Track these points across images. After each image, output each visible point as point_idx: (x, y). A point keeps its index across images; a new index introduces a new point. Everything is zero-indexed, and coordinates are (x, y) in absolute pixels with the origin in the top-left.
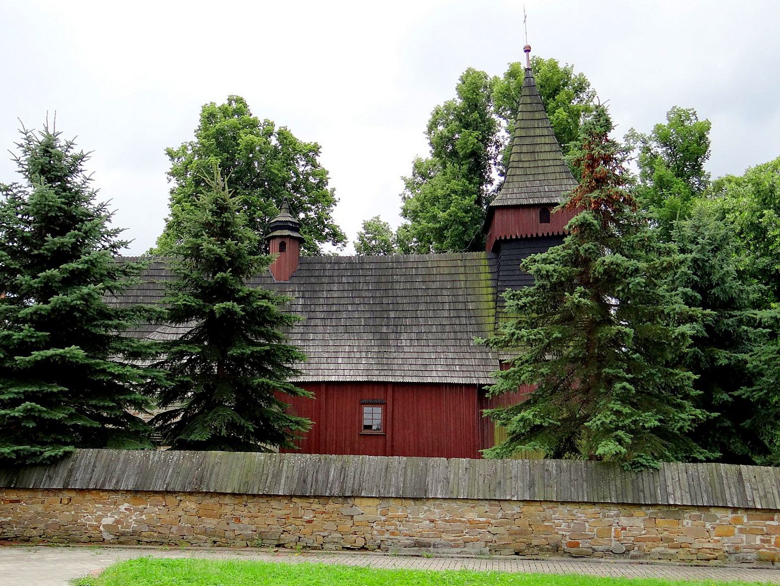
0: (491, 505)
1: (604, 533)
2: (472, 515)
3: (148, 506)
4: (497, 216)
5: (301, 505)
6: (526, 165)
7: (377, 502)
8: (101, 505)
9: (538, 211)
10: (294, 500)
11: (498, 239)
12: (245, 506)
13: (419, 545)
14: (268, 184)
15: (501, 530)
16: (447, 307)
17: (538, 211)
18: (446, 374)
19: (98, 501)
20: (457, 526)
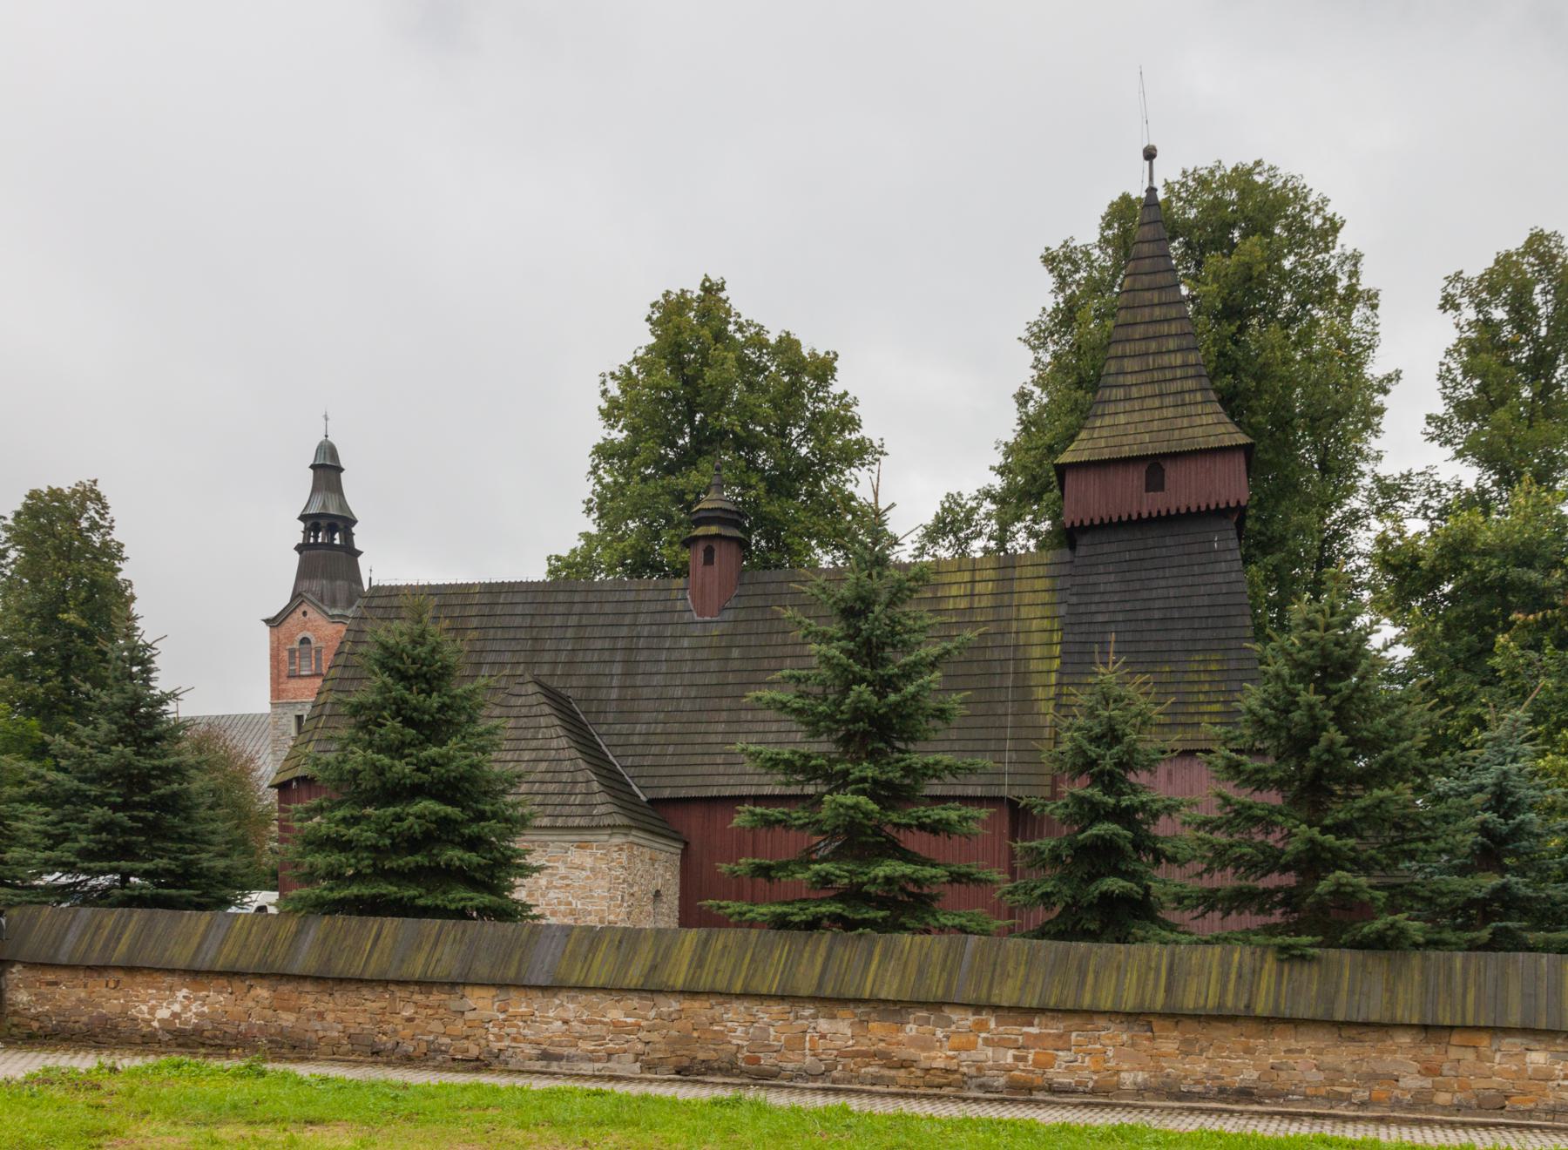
1: (795, 1043)
2: (616, 1014)
6: (1129, 379)
7: (493, 992)
9: (1143, 469)
13: (546, 1056)
15: (654, 1036)
16: (615, 682)
17: (1143, 469)
20: (597, 1030)
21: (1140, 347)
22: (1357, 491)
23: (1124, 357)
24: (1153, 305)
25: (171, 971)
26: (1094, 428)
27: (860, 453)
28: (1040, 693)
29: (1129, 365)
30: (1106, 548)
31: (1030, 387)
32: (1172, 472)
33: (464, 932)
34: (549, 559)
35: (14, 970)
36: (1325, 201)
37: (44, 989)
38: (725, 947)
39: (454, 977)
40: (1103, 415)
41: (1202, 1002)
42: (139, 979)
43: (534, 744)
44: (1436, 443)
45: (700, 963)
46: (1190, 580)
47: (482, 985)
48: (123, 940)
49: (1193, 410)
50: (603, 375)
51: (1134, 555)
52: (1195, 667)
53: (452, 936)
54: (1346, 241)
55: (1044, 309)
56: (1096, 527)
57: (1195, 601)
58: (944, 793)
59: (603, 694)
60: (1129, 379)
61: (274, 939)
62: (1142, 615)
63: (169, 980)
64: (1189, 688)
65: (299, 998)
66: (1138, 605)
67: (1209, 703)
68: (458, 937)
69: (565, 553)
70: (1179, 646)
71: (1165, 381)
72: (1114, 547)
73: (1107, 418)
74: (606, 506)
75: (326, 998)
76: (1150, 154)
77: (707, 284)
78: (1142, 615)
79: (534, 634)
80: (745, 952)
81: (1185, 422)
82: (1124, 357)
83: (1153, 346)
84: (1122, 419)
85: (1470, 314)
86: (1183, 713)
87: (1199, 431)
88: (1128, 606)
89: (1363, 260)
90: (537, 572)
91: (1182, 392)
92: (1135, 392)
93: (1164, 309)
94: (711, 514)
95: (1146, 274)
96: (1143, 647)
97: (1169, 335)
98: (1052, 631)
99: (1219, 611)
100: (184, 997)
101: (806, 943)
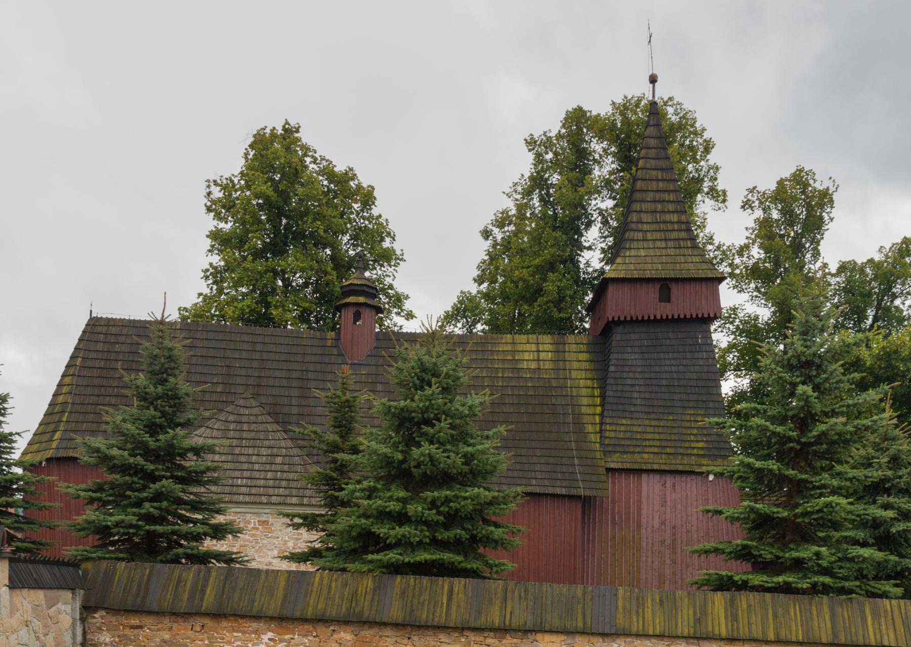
0: (687, 643)
3: (296, 636)
4: (611, 290)
5: (473, 639)
6: (645, 227)
8: (240, 634)
9: (658, 287)
10: (466, 633)
11: (610, 319)
12: (409, 638)
14: (366, 244)
16: (294, 402)
17: (658, 287)
18: (546, 482)
19: (236, 629)
21: (652, 206)
22: (844, 315)
23: (641, 211)
24: (658, 180)
25: (257, 617)
26: (625, 257)
27: (388, 257)
28: (590, 428)
29: (645, 217)
30: (633, 336)
31: (490, 227)
32: (675, 289)
33: (526, 591)
34: (179, 309)
35: (96, 615)
36: (704, 130)
37: (127, 632)
38: (749, 606)
39: (529, 626)
40: (630, 249)
41: (139, 600)
42: (224, 624)
43: (267, 443)
44: (736, 290)
45: (735, 618)
46: (685, 362)
47: (551, 632)
48: (208, 592)
49: (686, 251)
50: (208, 181)
51: (650, 343)
52: (688, 418)
53: (516, 593)
54: (713, 158)
55: (523, 175)
56: (634, 322)
57: (688, 376)
58: (542, 492)
59: (286, 410)
60: (645, 227)
61: (355, 594)
62: (654, 382)
63: (254, 625)
64: (685, 431)
65: (379, 641)
66: (653, 375)
67: (697, 441)
68: (523, 594)
69: (188, 306)
70: (679, 404)
71: (668, 231)
72: (636, 336)
73: (633, 251)
74: (486, 275)
75: (406, 641)
76: (653, 80)
77: (287, 126)
78: (654, 382)
79: (227, 363)
80: (767, 611)
81: (682, 259)
82: (641, 211)
83: (659, 207)
84: (643, 253)
85: (759, 213)
86: (681, 447)
87: (691, 266)
88: (646, 376)
89: (720, 171)
90: (173, 316)
91: (679, 239)
92: (649, 236)
93: (665, 184)
94: (359, 288)
95: (652, 159)
96: (656, 403)
97: (669, 201)
98: (593, 388)
99: (702, 383)
100: (269, 639)
101: (811, 604)
